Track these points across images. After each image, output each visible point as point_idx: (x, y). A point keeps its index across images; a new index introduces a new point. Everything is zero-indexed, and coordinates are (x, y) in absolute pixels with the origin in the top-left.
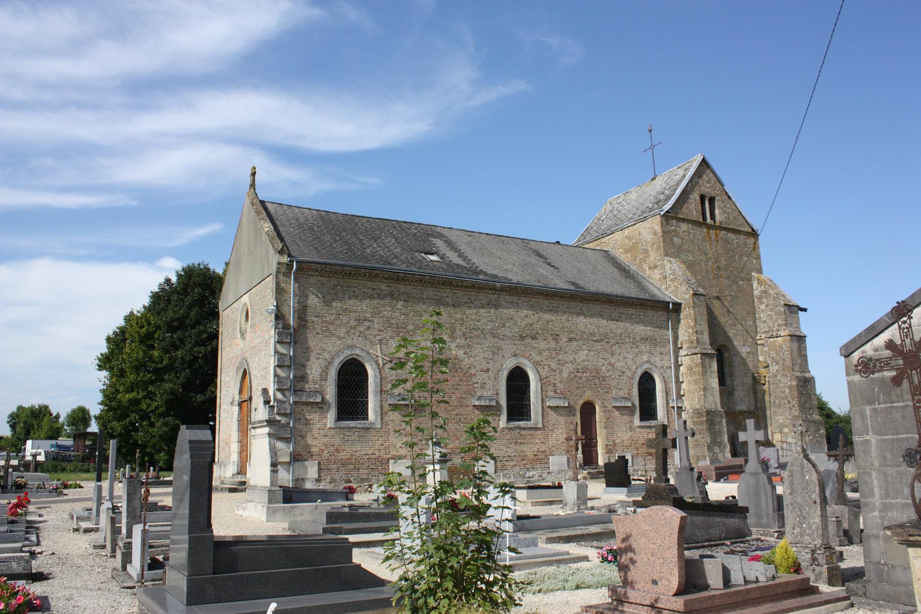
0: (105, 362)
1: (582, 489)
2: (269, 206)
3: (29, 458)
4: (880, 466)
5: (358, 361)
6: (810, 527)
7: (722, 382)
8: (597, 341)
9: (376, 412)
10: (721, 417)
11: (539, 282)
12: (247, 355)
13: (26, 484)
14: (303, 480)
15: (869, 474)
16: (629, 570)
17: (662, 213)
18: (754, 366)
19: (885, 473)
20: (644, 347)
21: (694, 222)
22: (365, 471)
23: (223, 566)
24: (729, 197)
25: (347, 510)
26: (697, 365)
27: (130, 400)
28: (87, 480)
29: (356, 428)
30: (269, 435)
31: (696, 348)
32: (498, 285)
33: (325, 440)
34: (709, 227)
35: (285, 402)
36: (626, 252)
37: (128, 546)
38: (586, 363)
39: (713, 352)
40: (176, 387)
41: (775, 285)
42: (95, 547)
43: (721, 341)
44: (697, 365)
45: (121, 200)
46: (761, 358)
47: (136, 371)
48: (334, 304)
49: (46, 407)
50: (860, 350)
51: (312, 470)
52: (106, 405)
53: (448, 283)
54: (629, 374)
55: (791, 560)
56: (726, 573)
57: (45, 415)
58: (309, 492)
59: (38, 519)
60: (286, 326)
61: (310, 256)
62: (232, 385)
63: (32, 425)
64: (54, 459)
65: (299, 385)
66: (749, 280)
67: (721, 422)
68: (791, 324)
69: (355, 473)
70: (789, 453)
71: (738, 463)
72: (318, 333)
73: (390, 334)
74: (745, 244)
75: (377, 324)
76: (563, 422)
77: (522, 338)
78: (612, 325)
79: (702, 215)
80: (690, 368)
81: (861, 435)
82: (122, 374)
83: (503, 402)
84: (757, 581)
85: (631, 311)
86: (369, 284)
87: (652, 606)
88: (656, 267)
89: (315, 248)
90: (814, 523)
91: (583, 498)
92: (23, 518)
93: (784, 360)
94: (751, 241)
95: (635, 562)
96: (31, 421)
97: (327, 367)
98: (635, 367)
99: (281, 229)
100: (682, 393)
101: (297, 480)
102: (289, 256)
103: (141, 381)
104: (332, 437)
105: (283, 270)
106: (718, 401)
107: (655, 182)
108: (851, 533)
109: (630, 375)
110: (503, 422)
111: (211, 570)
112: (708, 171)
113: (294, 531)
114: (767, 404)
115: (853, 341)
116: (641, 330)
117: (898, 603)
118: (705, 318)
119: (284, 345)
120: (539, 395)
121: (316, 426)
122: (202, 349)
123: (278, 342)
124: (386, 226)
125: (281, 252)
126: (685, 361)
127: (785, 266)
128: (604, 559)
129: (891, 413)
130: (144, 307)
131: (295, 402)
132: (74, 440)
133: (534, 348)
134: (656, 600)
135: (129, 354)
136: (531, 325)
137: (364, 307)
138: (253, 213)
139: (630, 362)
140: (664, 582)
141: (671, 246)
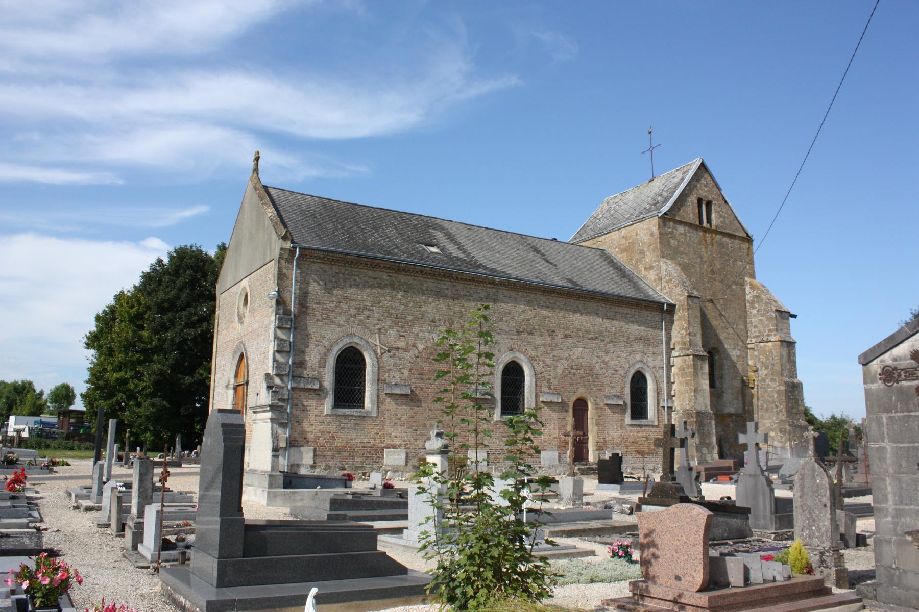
0: (93, 341)
1: (578, 485)
2: (272, 191)
3: (11, 433)
4: (895, 472)
5: (357, 350)
6: (819, 530)
7: (712, 385)
8: (592, 339)
9: (372, 400)
10: (711, 418)
11: (537, 278)
12: (245, 339)
13: (17, 460)
14: (298, 465)
15: (884, 480)
16: (651, 565)
17: (660, 215)
18: (744, 369)
19: (900, 480)
20: (638, 347)
21: (691, 225)
22: (360, 459)
23: (250, 551)
24: (726, 202)
25: (350, 497)
26: (688, 366)
27: (117, 379)
28: (73, 457)
29: (353, 416)
30: (272, 420)
31: (688, 349)
32: (497, 279)
33: (321, 427)
34: (705, 230)
35: (283, 388)
36: (622, 251)
37: (140, 527)
38: (581, 360)
39: (705, 354)
40: (165, 368)
41: (767, 290)
42: (99, 525)
43: (712, 344)
44: (688, 366)
45: (108, 178)
46: (750, 362)
47: (125, 351)
48: (335, 292)
49: (30, 383)
50: (879, 359)
51: (307, 456)
52: (93, 384)
53: (448, 276)
54: (622, 372)
55: (804, 561)
56: (746, 571)
57: (28, 392)
58: (304, 477)
59: (34, 495)
60: (287, 312)
61: (312, 243)
62: (227, 368)
63: (14, 401)
64: (38, 435)
65: (298, 371)
66: (742, 285)
67: (710, 423)
68: (782, 330)
69: (350, 460)
70: (775, 456)
71: (727, 465)
72: (318, 320)
73: (389, 323)
74: (740, 248)
75: (377, 313)
76: (556, 418)
77: (519, 333)
78: (608, 324)
79: (699, 218)
80: (682, 369)
81: (876, 442)
82: (111, 353)
83: (498, 395)
84: (774, 581)
85: (626, 310)
86: (370, 273)
87: (675, 602)
88: (651, 268)
89: (318, 235)
90: (824, 525)
91: (578, 493)
92: (21, 494)
93: (773, 365)
94: (745, 246)
95: (658, 557)
96: (19, 396)
97: (325, 355)
98: (627, 366)
99: (284, 215)
100: (673, 393)
101: (292, 466)
102: (292, 242)
103: (130, 361)
104: (329, 423)
105: (286, 256)
106: (708, 403)
107: (653, 183)
108: (847, 537)
109: (622, 374)
110: (497, 415)
111: (240, 553)
112: (706, 175)
113: (296, 516)
114: (755, 407)
115: (872, 350)
116: (635, 329)
117: (909, 607)
118: (699, 320)
119: (284, 331)
120: (534, 389)
121: (313, 412)
122: (192, 331)
123: (278, 328)
124: (386, 216)
125: (284, 238)
126: (677, 361)
127: (775, 273)
128: (615, 554)
129: (907, 422)
130: (135, 287)
131: (292, 388)
132: (59, 417)
133: (529, 343)
134: (680, 596)
135: (118, 334)
136: (528, 320)
137: (364, 296)
138: (256, 198)
139: (623, 361)
140: (688, 578)
141: (667, 248)
